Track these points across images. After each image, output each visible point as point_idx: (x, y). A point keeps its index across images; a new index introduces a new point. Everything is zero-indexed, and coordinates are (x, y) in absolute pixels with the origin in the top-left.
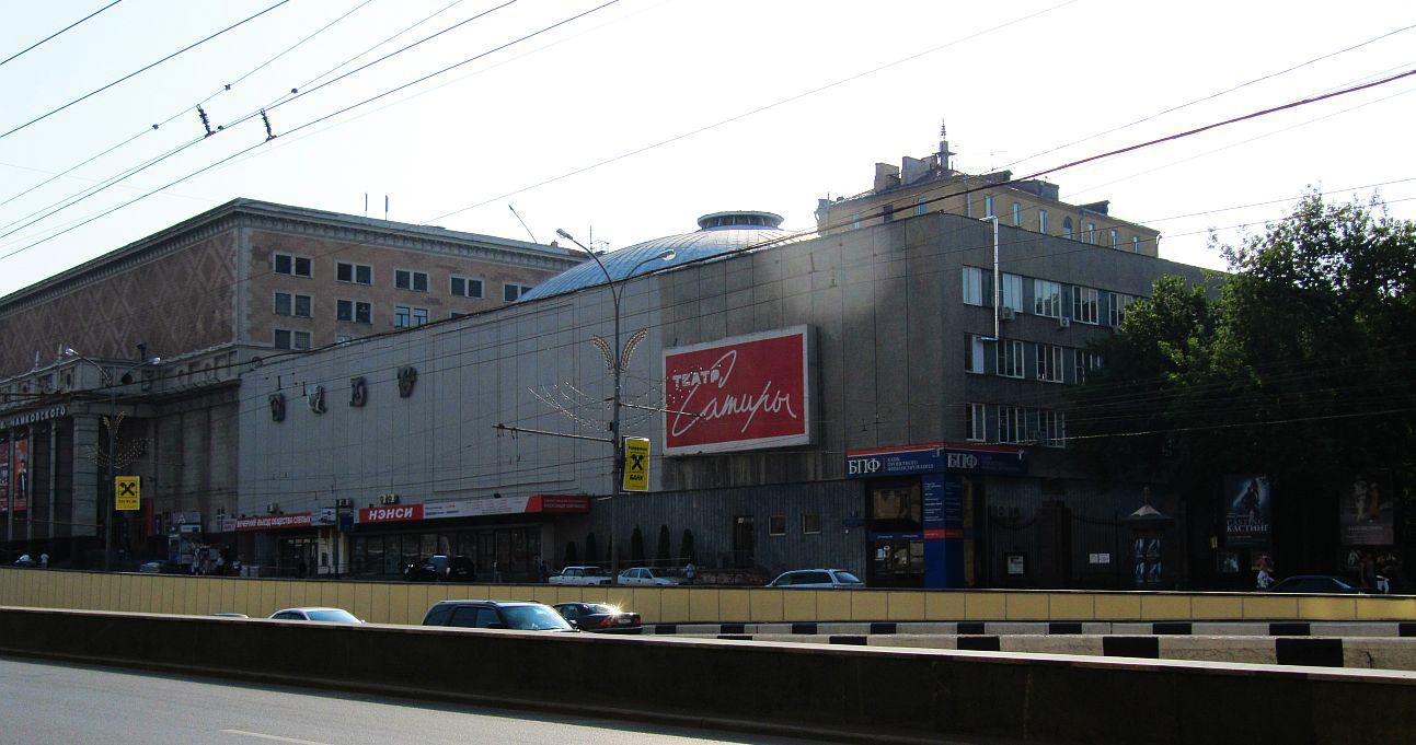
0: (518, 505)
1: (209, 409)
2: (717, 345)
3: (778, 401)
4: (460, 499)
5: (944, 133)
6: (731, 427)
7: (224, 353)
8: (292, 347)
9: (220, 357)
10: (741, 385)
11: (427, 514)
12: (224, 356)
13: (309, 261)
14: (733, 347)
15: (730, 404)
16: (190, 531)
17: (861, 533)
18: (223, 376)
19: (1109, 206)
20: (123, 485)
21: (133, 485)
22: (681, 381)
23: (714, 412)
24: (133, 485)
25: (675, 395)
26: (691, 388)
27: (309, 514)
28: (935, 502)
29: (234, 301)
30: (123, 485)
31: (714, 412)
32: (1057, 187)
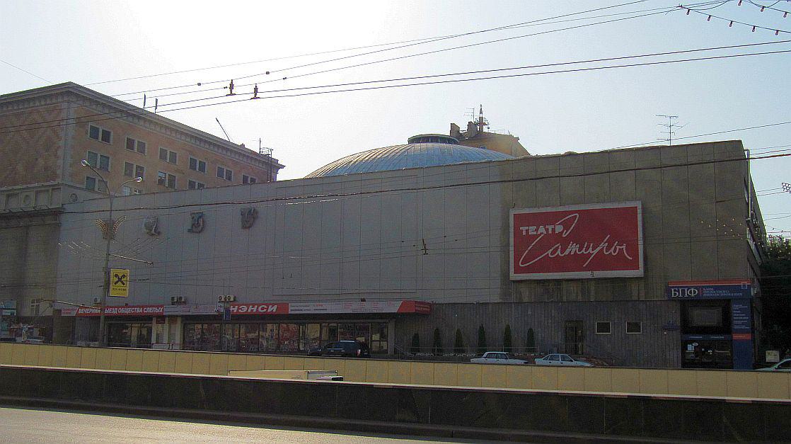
0: (394, 308)
1: (27, 227)
2: (561, 209)
3: (616, 248)
4: (327, 301)
5: (481, 112)
6: (576, 262)
7: (47, 188)
8: (96, 189)
9: (41, 191)
10: (576, 237)
11: (292, 310)
12: (48, 191)
13: (109, 132)
14: (576, 212)
15: (573, 248)
16: (9, 314)
17: (677, 335)
18: (43, 202)
19: (280, 171)
20: (116, 276)
21: (124, 276)
22: (527, 231)
23: (559, 252)
24: (124, 276)
25: (522, 241)
26: (535, 237)
27: (162, 306)
28: (743, 317)
29: (60, 153)
30: (116, 276)
31: (559, 252)
32: (740, 141)
